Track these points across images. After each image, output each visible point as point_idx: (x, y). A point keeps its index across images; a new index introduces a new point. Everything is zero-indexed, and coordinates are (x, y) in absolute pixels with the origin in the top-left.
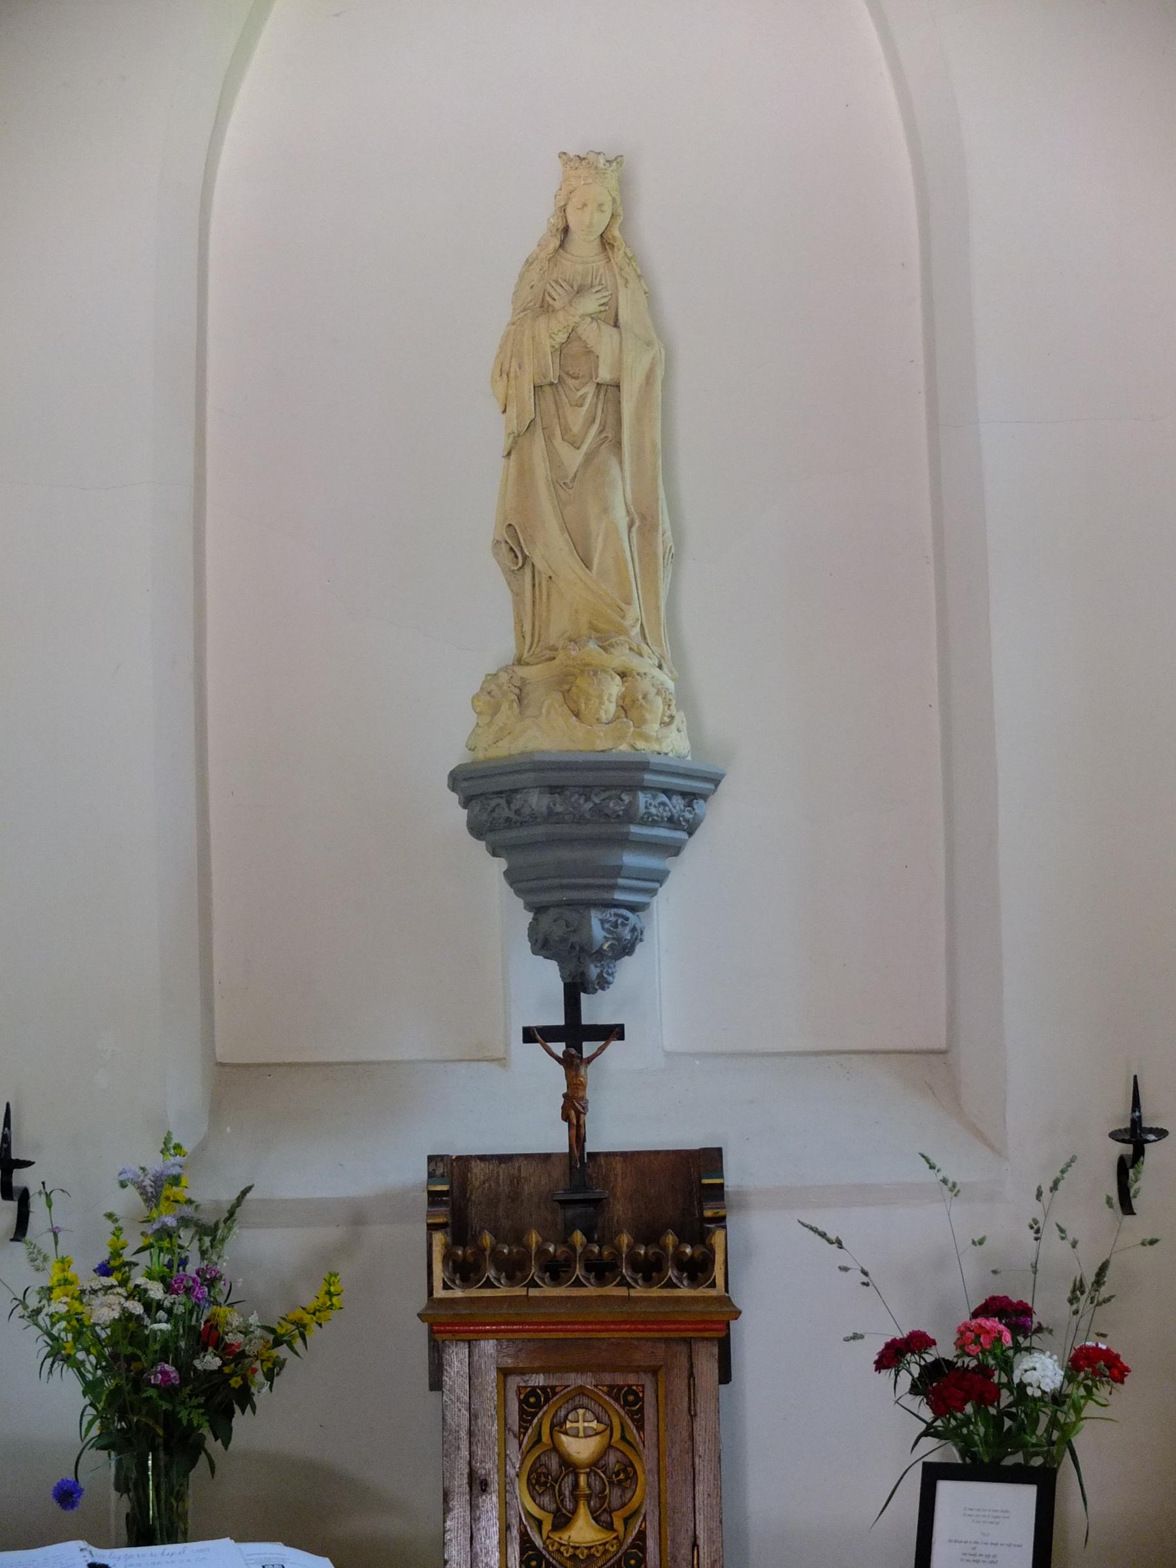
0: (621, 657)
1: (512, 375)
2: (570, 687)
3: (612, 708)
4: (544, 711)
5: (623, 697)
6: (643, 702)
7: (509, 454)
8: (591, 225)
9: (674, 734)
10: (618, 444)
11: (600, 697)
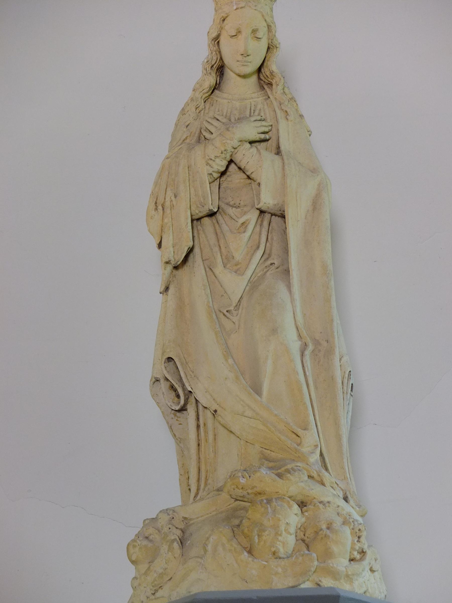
0: (297, 485)
1: (168, 204)
2: (241, 516)
3: (291, 540)
4: (209, 548)
5: (303, 528)
6: (328, 532)
7: (167, 289)
8: (246, 55)
9: (367, 574)
10: (287, 272)
11: (276, 527)
